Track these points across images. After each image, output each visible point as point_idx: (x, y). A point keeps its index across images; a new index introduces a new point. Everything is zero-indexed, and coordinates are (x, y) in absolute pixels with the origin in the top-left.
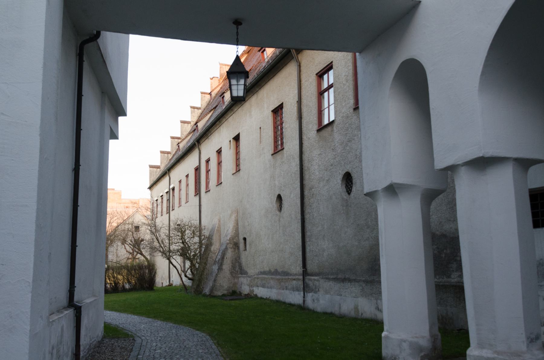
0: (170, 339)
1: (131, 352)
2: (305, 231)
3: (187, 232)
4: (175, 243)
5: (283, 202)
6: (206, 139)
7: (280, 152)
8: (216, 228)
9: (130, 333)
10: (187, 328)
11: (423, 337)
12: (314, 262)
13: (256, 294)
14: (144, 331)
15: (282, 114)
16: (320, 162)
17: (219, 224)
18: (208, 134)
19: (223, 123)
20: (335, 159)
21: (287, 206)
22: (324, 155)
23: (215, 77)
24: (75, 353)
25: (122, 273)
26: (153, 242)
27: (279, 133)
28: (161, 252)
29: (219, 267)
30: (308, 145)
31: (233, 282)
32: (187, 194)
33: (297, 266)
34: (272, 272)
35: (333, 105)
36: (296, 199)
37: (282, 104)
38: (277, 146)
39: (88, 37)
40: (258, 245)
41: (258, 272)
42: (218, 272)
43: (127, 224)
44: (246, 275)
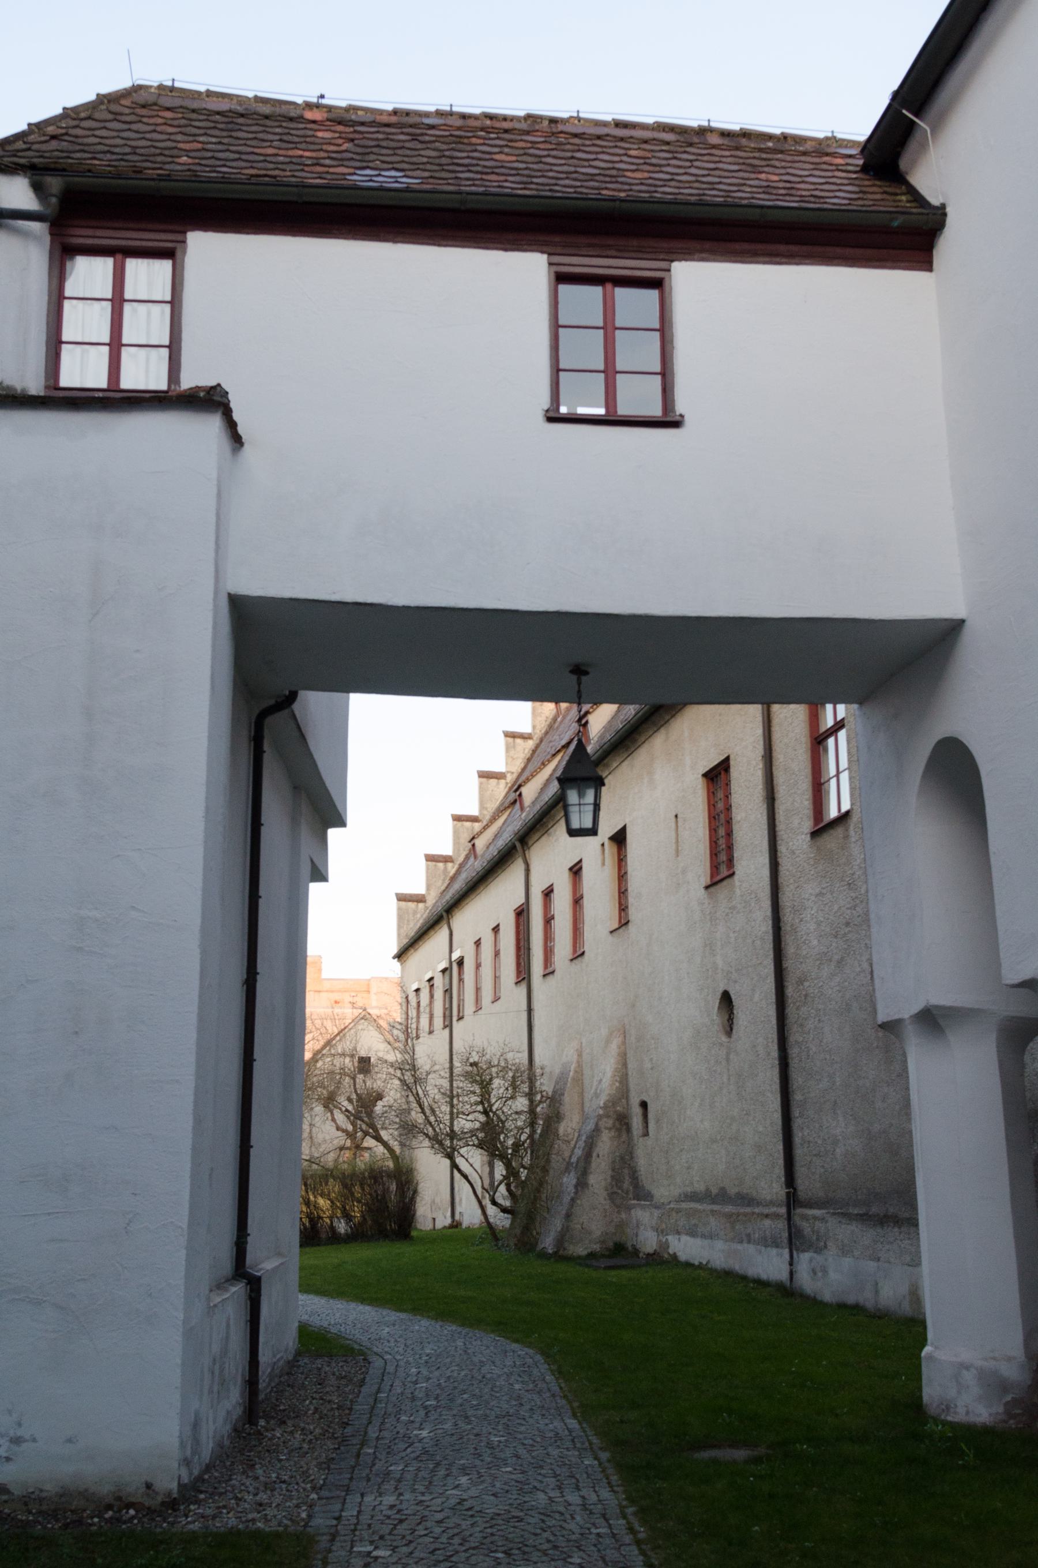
0: (448, 1360)
1: (361, 1386)
2: (791, 1090)
3: (496, 1082)
4: (464, 1114)
5: (735, 1012)
6: (543, 835)
7: (725, 883)
9: (356, 1347)
10: (492, 1335)
11: (1009, 1359)
12: (814, 1170)
13: (675, 1253)
14: (389, 1341)
15: (728, 784)
16: (820, 912)
17: (578, 1062)
20: (854, 907)
22: (829, 896)
24: (247, 1378)
25: (329, 1192)
26: (409, 1111)
27: (722, 832)
28: (430, 1139)
29: (578, 1179)
30: (791, 868)
32: (496, 978)
35: (847, 771)
37: (728, 759)
38: (719, 864)
39: (272, 702)
42: (576, 1193)
43: (339, 1054)
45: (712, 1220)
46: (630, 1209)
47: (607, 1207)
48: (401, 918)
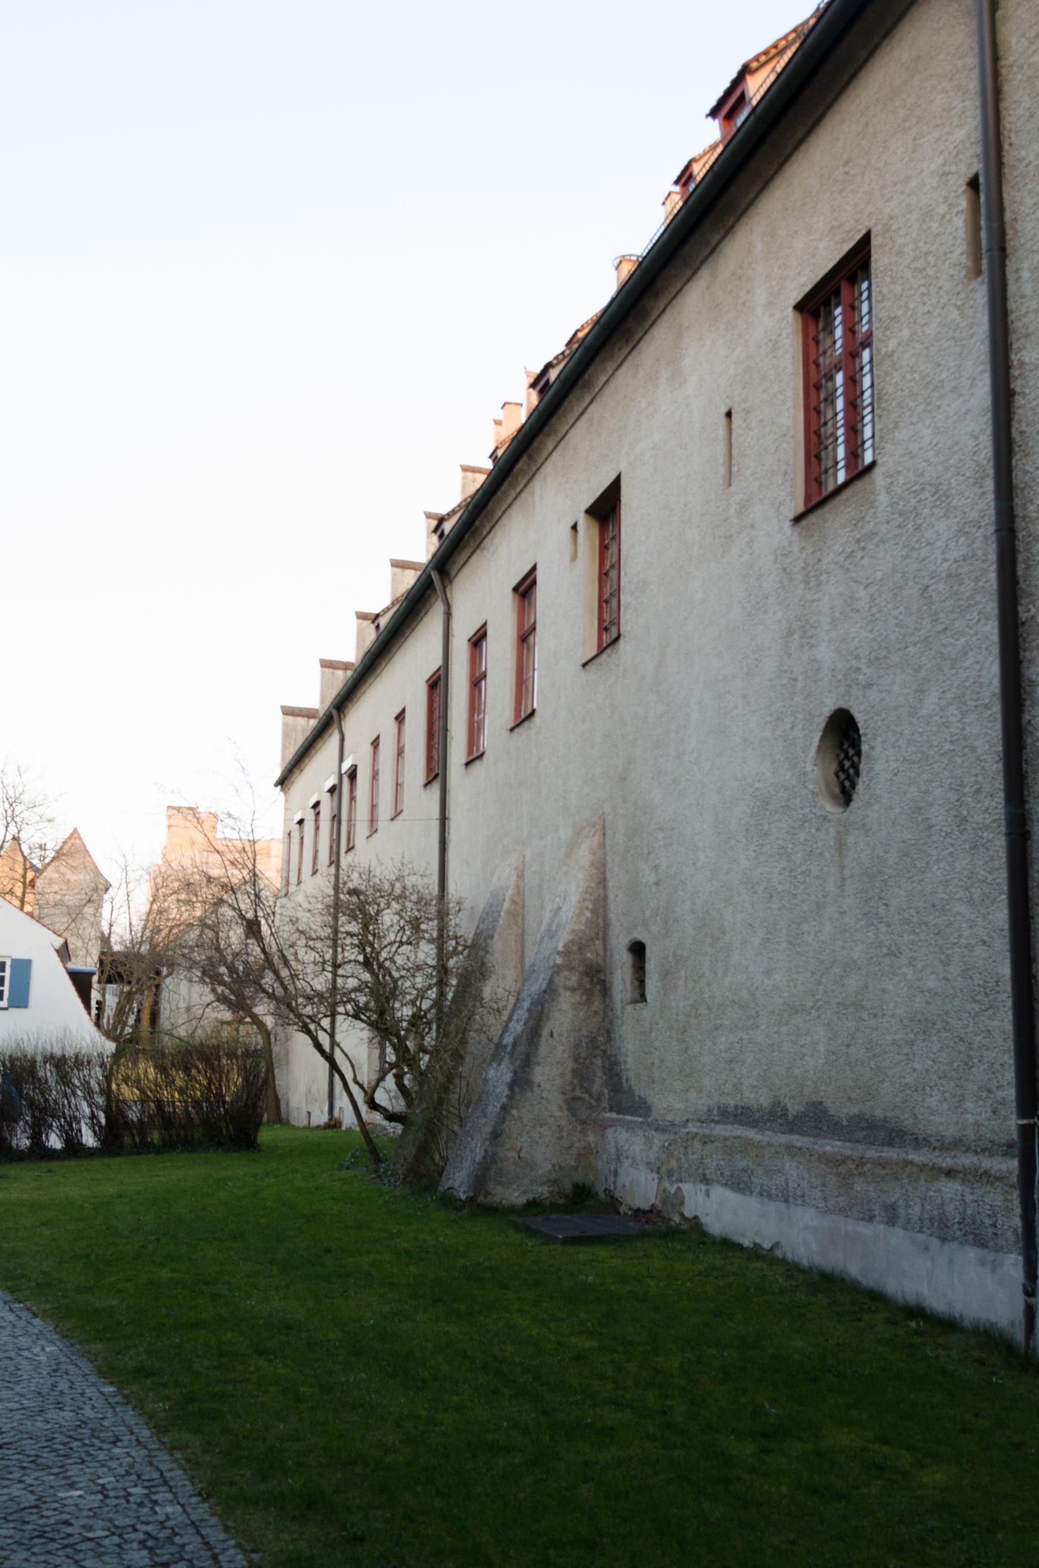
6: (474, 552)
8: (506, 905)
17: (518, 887)
18: (483, 525)
19: (546, 459)
21: (893, 765)
23: (509, 403)
29: (515, 1073)
31: (577, 1145)
33: (963, 1099)
34: (790, 1117)
36: (964, 714)
40: (707, 973)
41: (705, 1109)
42: (510, 1097)
44: (640, 1116)
45: (789, 1165)
46: (604, 1128)
47: (563, 1122)
48: (286, 736)
